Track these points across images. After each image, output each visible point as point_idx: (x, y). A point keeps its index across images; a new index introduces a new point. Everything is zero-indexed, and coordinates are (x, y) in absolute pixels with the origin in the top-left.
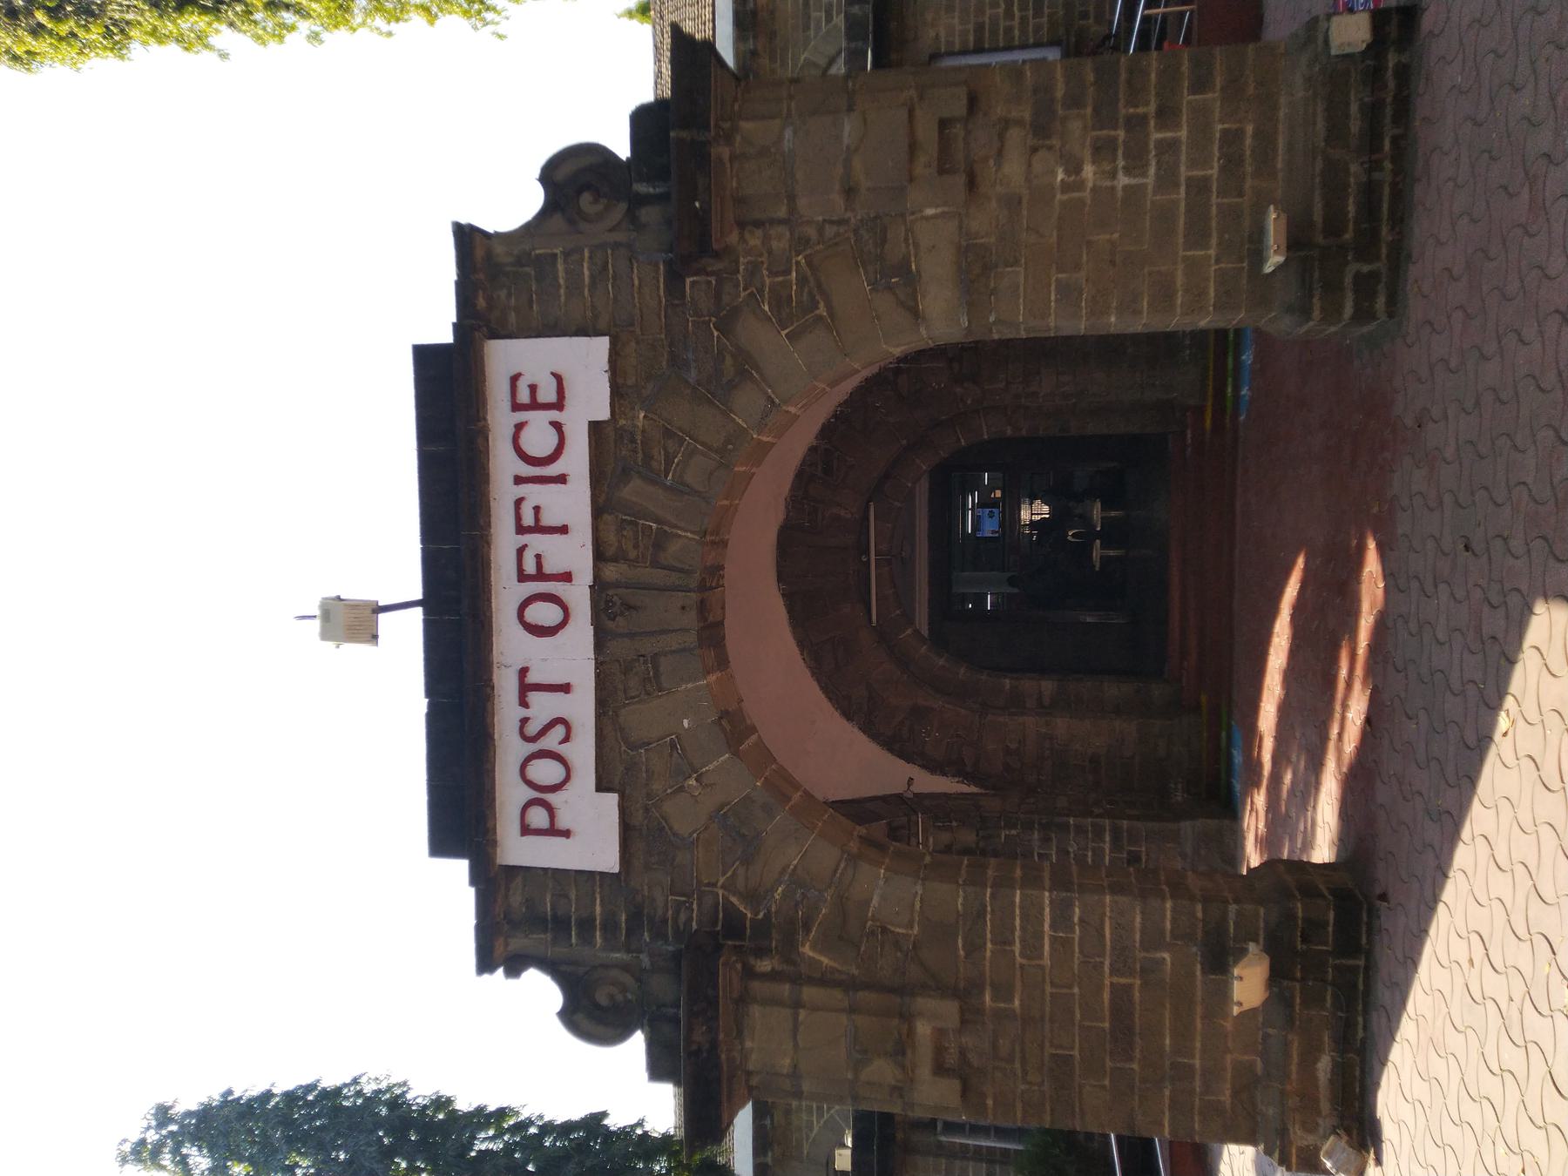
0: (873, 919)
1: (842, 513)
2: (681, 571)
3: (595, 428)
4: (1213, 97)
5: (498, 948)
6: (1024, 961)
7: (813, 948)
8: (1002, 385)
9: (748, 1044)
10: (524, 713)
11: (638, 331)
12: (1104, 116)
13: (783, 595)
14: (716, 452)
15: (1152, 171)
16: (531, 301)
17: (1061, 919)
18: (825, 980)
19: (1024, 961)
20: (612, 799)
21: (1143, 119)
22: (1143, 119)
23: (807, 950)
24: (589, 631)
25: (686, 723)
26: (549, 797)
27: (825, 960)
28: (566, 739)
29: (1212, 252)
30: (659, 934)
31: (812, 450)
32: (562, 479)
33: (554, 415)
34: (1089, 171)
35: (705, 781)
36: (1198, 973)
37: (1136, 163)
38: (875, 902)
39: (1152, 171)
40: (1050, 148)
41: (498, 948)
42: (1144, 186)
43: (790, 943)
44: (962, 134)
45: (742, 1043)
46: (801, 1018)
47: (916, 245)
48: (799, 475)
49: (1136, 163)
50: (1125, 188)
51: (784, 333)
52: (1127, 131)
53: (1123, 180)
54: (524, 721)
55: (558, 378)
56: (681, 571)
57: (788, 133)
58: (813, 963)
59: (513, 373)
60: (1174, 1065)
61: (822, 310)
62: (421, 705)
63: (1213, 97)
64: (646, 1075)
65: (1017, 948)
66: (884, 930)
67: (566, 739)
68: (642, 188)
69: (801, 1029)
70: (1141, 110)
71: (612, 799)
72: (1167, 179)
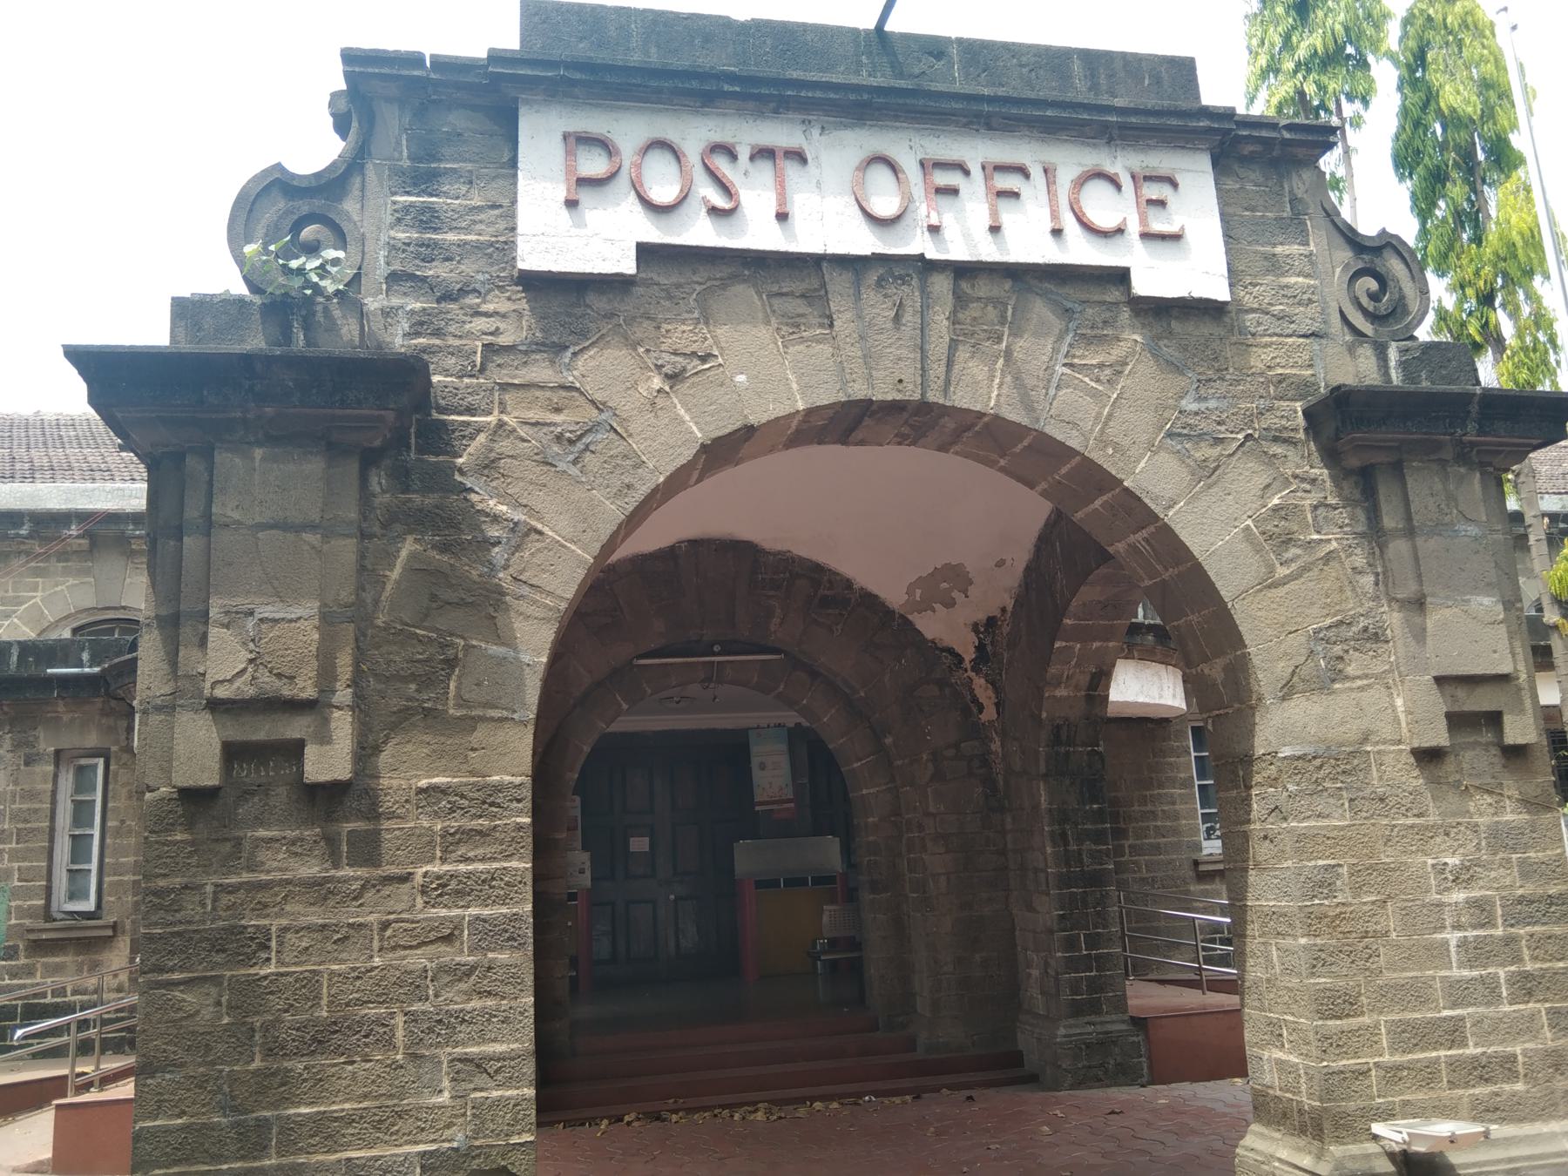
0: (468, 648)
1: (776, 620)
2: (948, 382)
3: (1121, 276)
4: (1548, 1038)
5: (380, 89)
6: (419, 879)
7: (413, 556)
8: (932, 809)
9: (258, 453)
10: (744, 153)
11: (1234, 339)
12: (1523, 909)
13: (672, 548)
14: (1102, 431)
15: (1466, 973)
16: (1253, 209)
17: (490, 934)
18: (368, 574)
19: (419, 879)
20: (627, 265)
21: (1517, 959)
22: (1517, 959)
23: (408, 547)
24: (866, 251)
25: (741, 378)
26: (623, 182)
27: (395, 574)
28: (714, 211)
29: (1386, 1058)
30: (420, 325)
31: (848, 584)
32: (1057, 233)
33: (1134, 228)
34: (1458, 896)
35: (660, 402)
36: (422, 1148)
37: (1475, 953)
38: (494, 649)
39: (1466, 973)
40: (1478, 848)
41: (380, 89)
42: (1451, 968)
43: (420, 521)
44: (1483, 740)
45: (259, 444)
46: (307, 536)
47: (1361, 689)
48: (818, 568)
49: (1475, 953)
50: (1446, 943)
51: (1249, 522)
52: (1501, 939)
53: (1453, 937)
54: (732, 156)
55: (1176, 237)
56: (948, 382)
57: (1473, 530)
58: (390, 557)
59: (1179, 178)
60: (263, 1125)
61: (1282, 571)
62: (741, 14)
63: (1548, 1038)
64: (186, 293)
65: (436, 868)
66: (451, 663)
67: (714, 211)
68: (1393, 355)
69: (290, 536)
70: (1526, 953)
71: (627, 265)
72: (1458, 993)
